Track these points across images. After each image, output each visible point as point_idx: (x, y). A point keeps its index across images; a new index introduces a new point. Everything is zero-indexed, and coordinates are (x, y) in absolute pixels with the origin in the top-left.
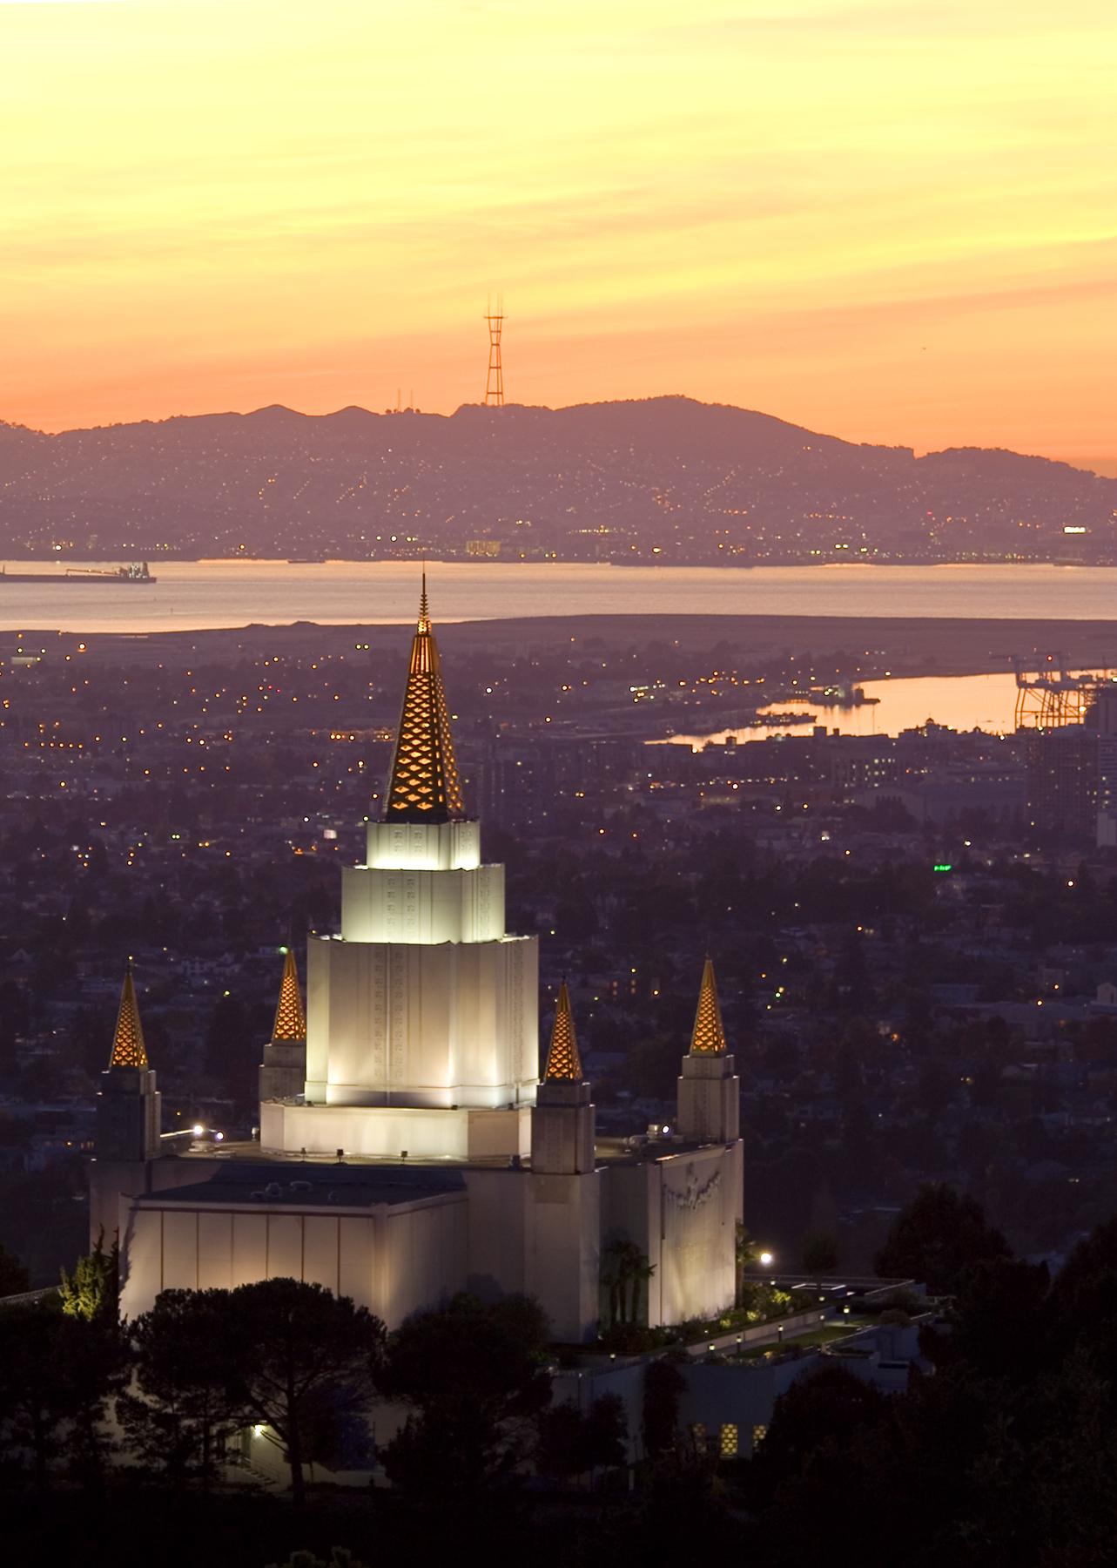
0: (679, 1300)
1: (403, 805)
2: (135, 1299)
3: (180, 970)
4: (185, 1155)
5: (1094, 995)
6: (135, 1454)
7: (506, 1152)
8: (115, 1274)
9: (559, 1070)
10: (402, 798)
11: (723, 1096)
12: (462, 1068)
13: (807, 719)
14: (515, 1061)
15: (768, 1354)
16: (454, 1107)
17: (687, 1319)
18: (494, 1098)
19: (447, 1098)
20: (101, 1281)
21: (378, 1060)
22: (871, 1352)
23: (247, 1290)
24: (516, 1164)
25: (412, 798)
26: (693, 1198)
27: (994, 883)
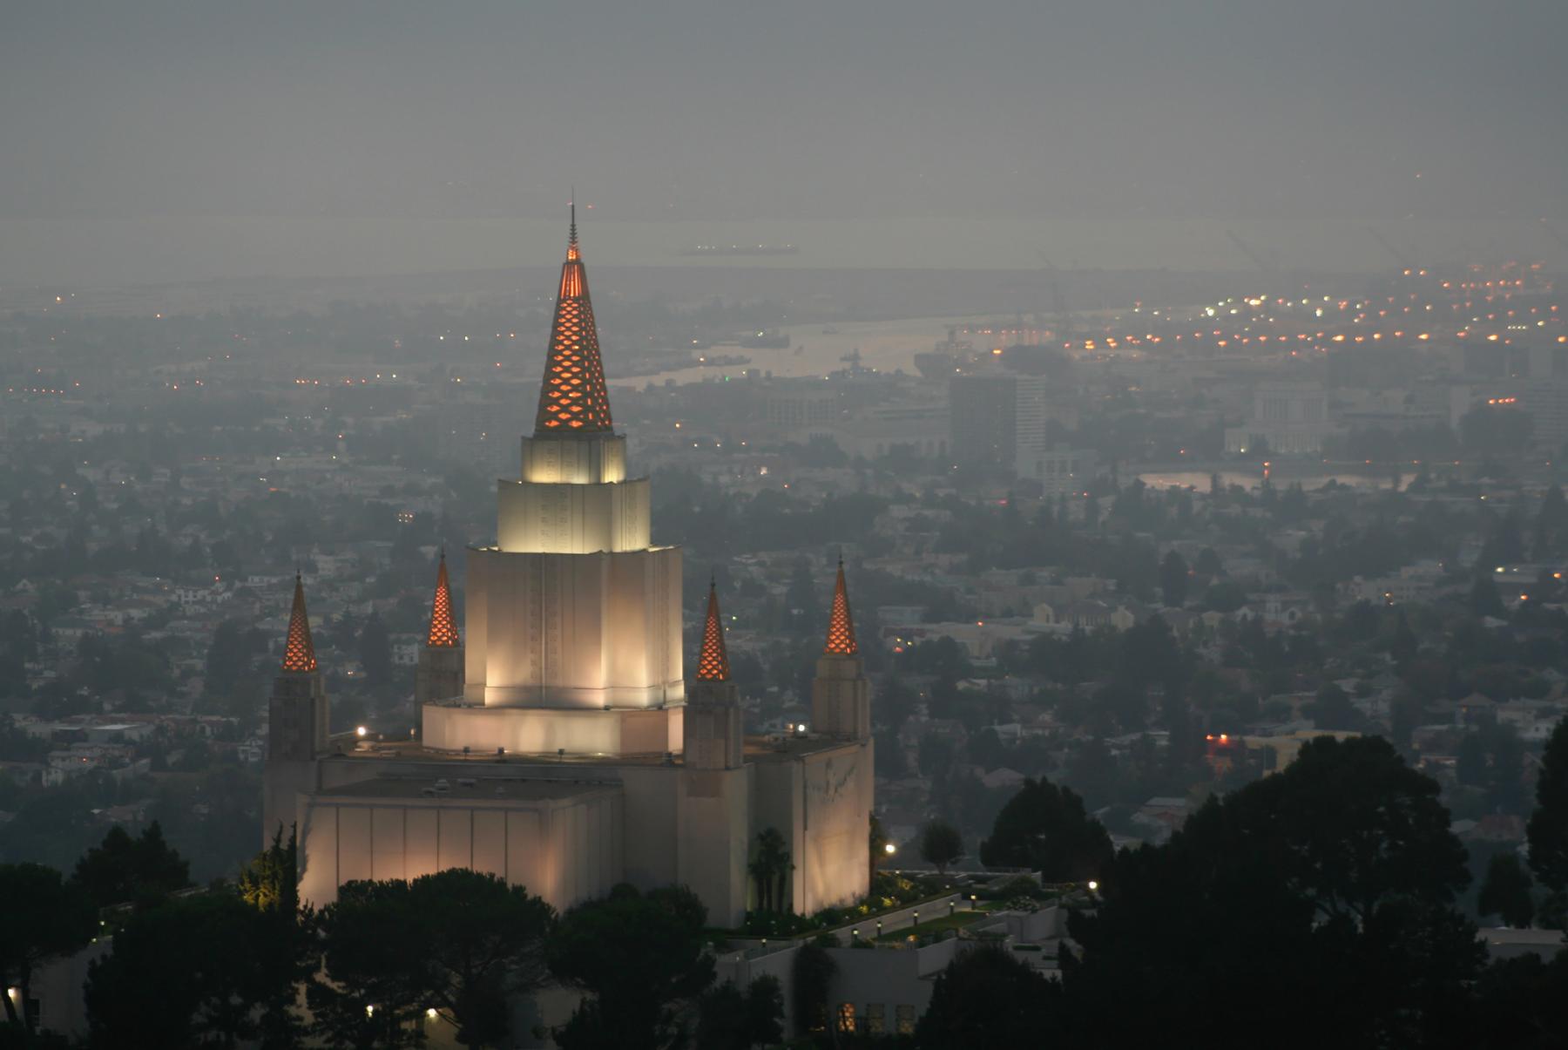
0: (820, 888)
1: (554, 423)
2: (315, 886)
3: (174, 598)
4: (351, 754)
5: (1031, 616)
6: (324, 1038)
8: (294, 867)
9: (709, 672)
10: (555, 416)
13: (742, 361)
15: (911, 938)
16: (607, 708)
17: (826, 906)
18: (644, 698)
19: (600, 699)
20: (281, 874)
21: (534, 663)
22: (1005, 935)
23: (425, 881)
24: (669, 761)
25: (563, 416)
26: (832, 792)
27: (929, 513)
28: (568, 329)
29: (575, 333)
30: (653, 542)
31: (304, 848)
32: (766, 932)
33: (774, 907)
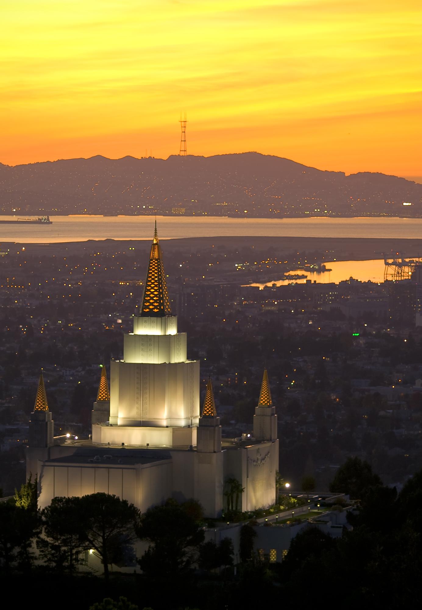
0: (254, 501)
1: (147, 310)
2: (44, 500)
4: (63, 445)
8: (36, 491)
10: (147, 307)
12: (170, 412)
13: (304, 277)
14: (191, 409)
16: (167, 427)
19: (165, 423)
20: (31, 494)
21: (137, 408)
23: (87, 498)
25: (151, 307)
26: (259, 462)
28: (153, 271)
29: (156, 273)
30: (188, 358)
31: (40, 483)
32: (231, 521)
33: (234, 509)
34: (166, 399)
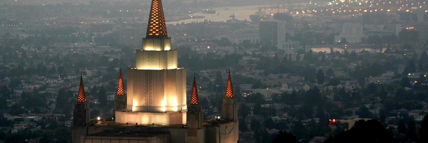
1: (151, 34)
3: (48, 82)
5: (281, 87)
7: (179, 123)
9: (194, 102)
10: (151, 32)
11: (233, 108)
12: (167, 101)
13: (203, 17)
14: (181, 100)
16: (166, 112)
18: (175, 109)
21: (146, 100)
24: (183, 126)
25: (154, 32)
26: (227, 135)
27: (254, 59)
30: (178, 67)
34: (165, 93)
